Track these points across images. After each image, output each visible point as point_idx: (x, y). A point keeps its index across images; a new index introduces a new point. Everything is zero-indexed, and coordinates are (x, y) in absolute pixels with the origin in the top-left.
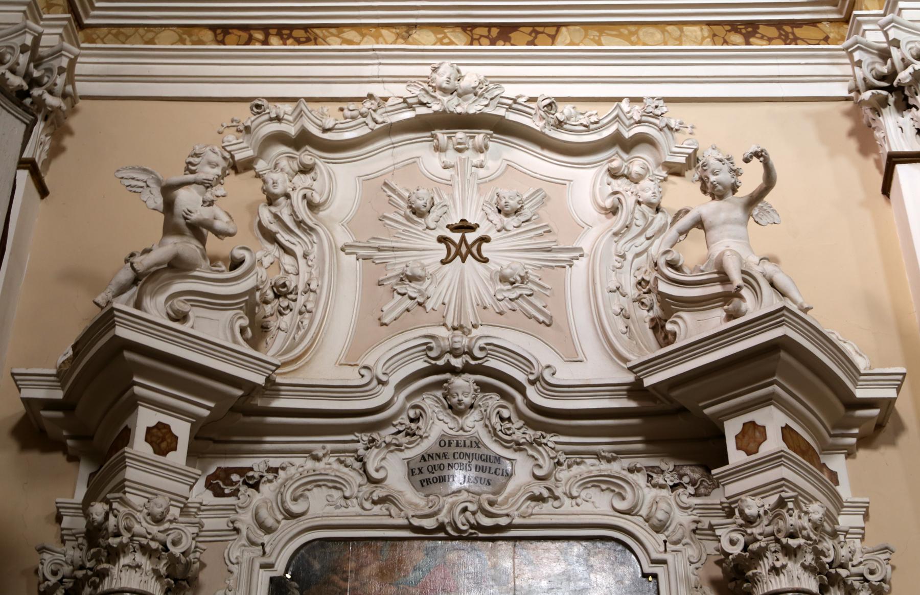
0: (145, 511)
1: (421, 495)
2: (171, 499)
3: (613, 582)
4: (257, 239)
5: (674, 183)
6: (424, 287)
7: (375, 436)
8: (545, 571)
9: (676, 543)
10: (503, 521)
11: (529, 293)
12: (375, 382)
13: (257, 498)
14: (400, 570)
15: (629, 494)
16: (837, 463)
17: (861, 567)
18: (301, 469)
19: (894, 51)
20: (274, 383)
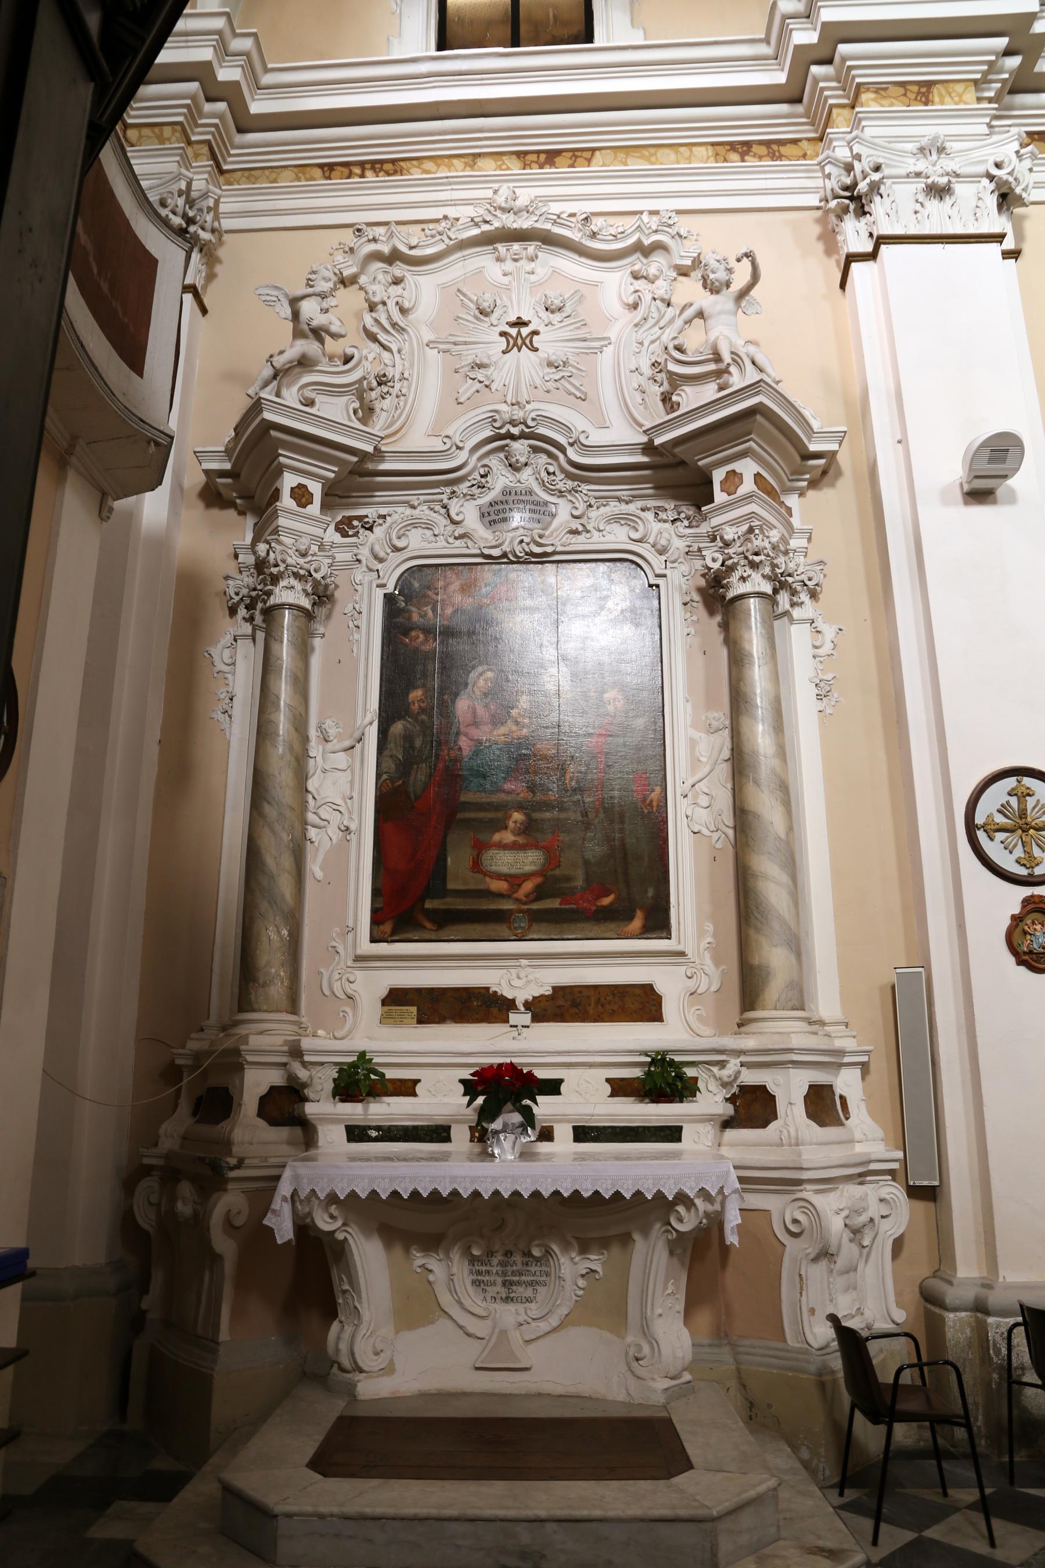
0: (294, 548)
1: (490, 531)
2: (312, 539)
3: (627, 591)
4: (363, 339)
5: (681, 282)
6: (489, 373)
7: (455, 488)
8: (579, 584)
9: (673, 562)
10: (549, 549)
11: (569, 374)
12: (454, 448)
13: (371, 537)
14: (475, 586)
15: (641, 527)
16: (792, 501)
17: (803, 575)
18: (402, 516)
19: (856, 164)
20: (380, 451)
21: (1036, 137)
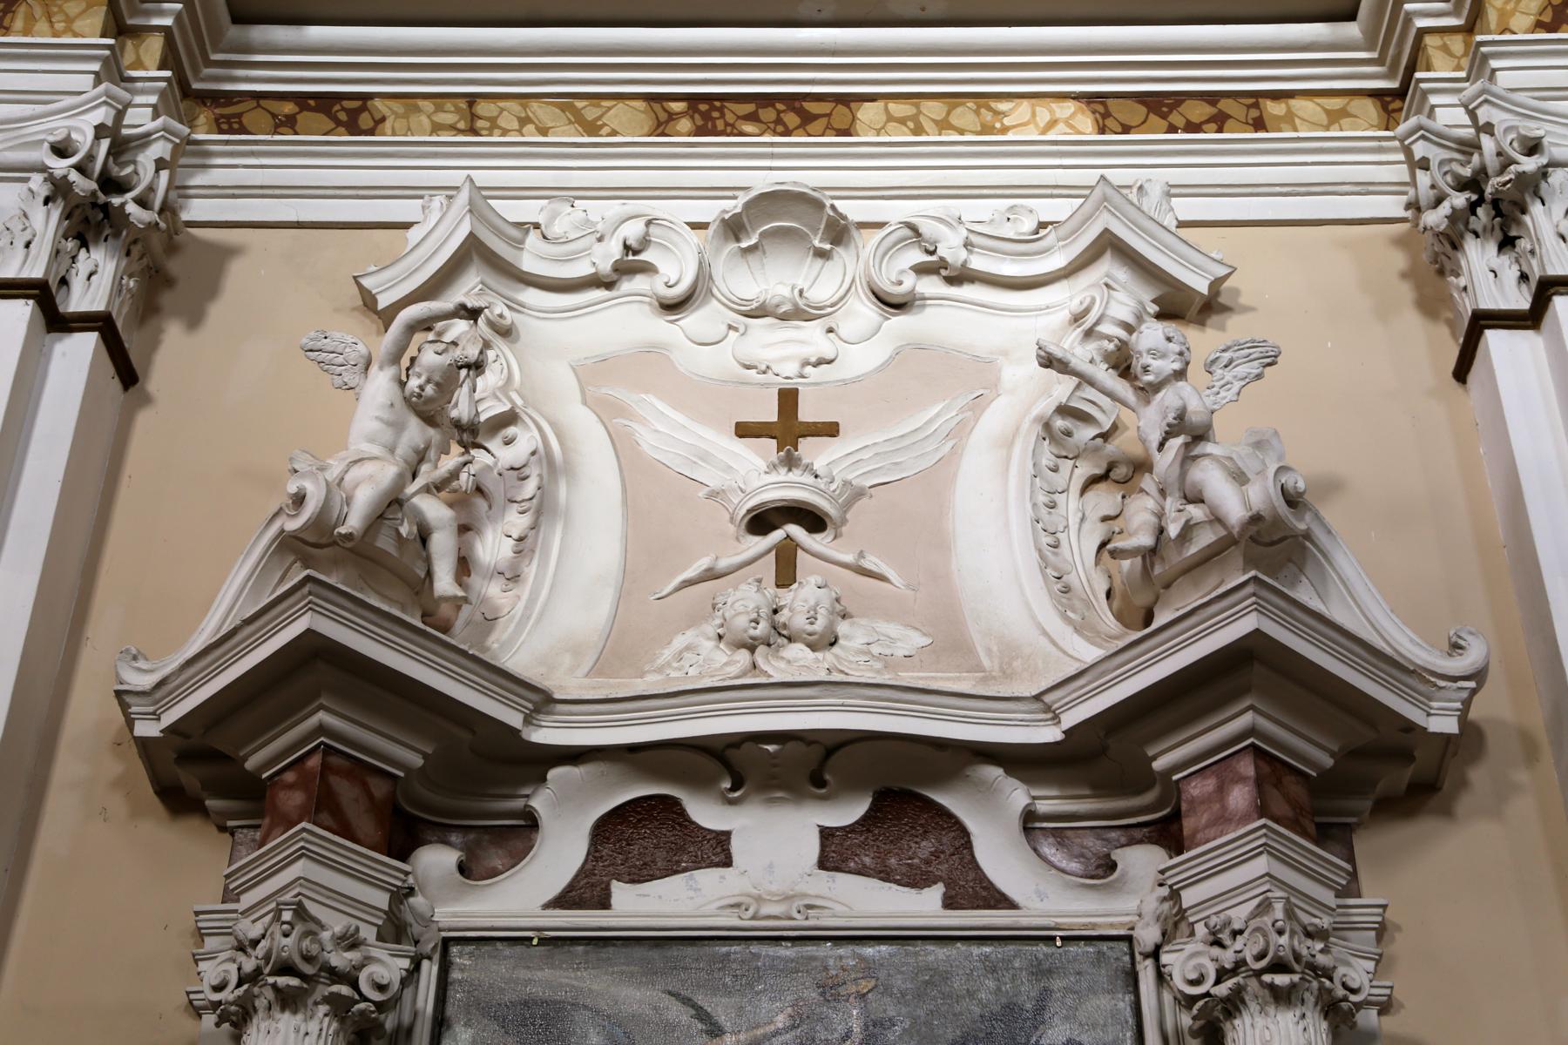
21: (312, 102)
